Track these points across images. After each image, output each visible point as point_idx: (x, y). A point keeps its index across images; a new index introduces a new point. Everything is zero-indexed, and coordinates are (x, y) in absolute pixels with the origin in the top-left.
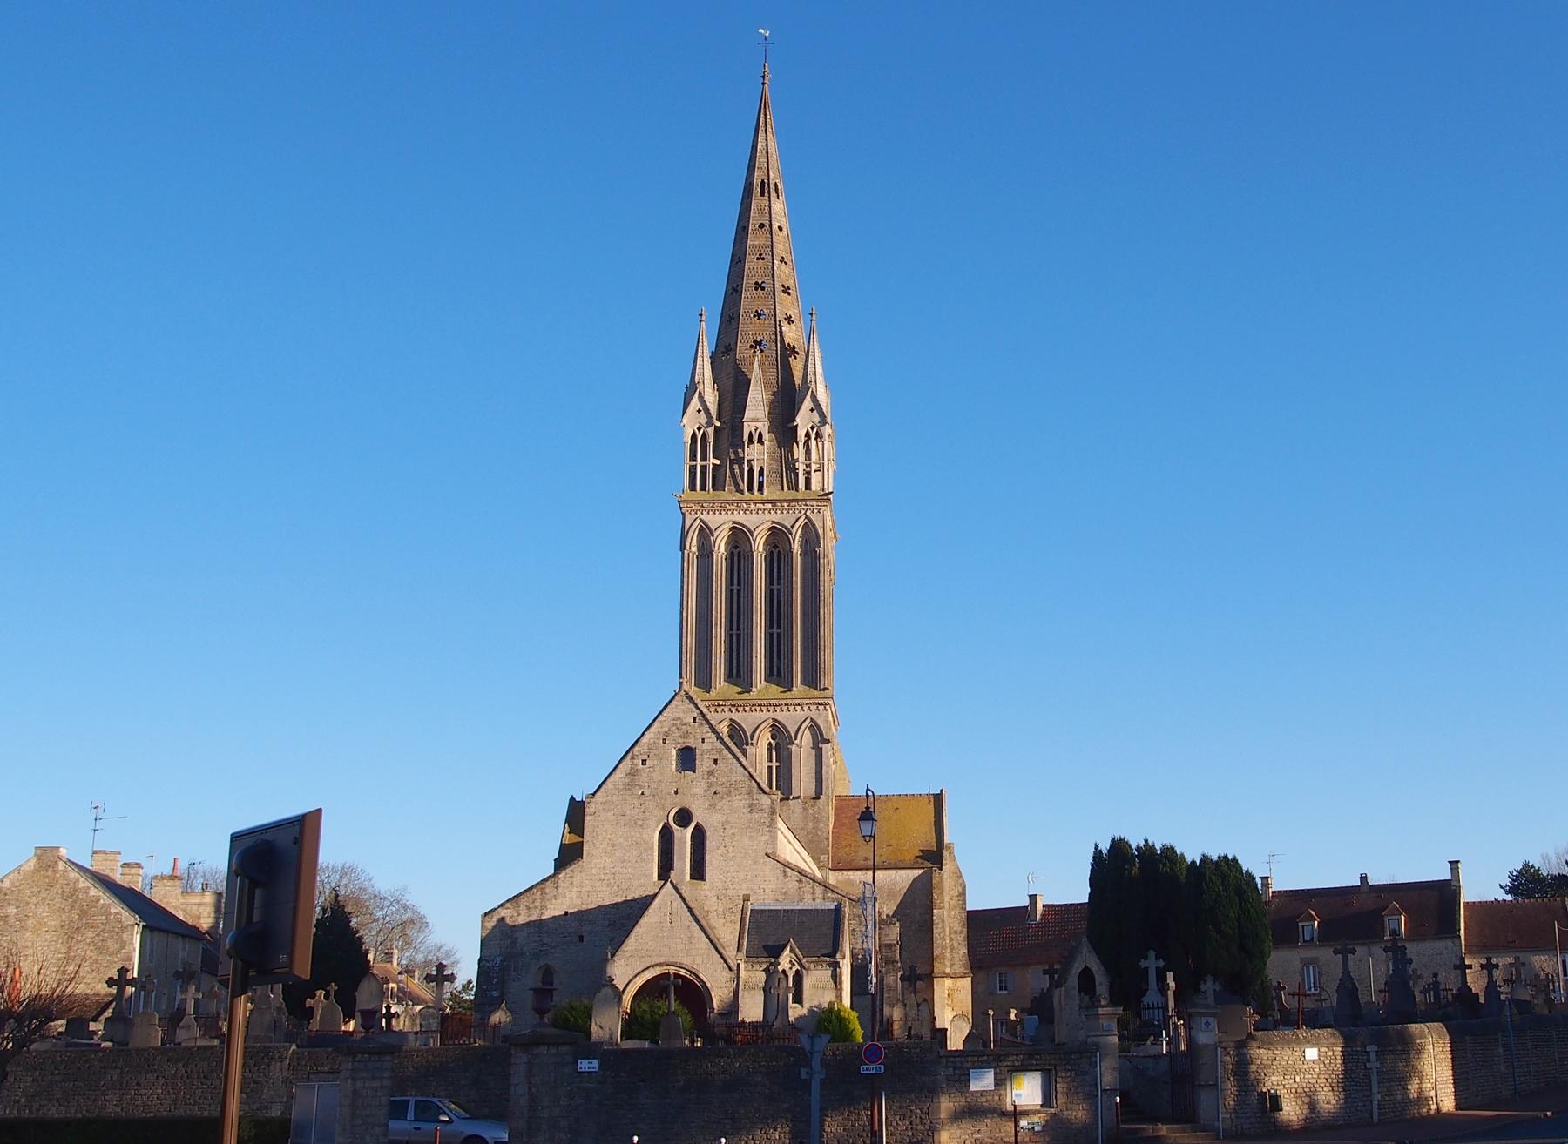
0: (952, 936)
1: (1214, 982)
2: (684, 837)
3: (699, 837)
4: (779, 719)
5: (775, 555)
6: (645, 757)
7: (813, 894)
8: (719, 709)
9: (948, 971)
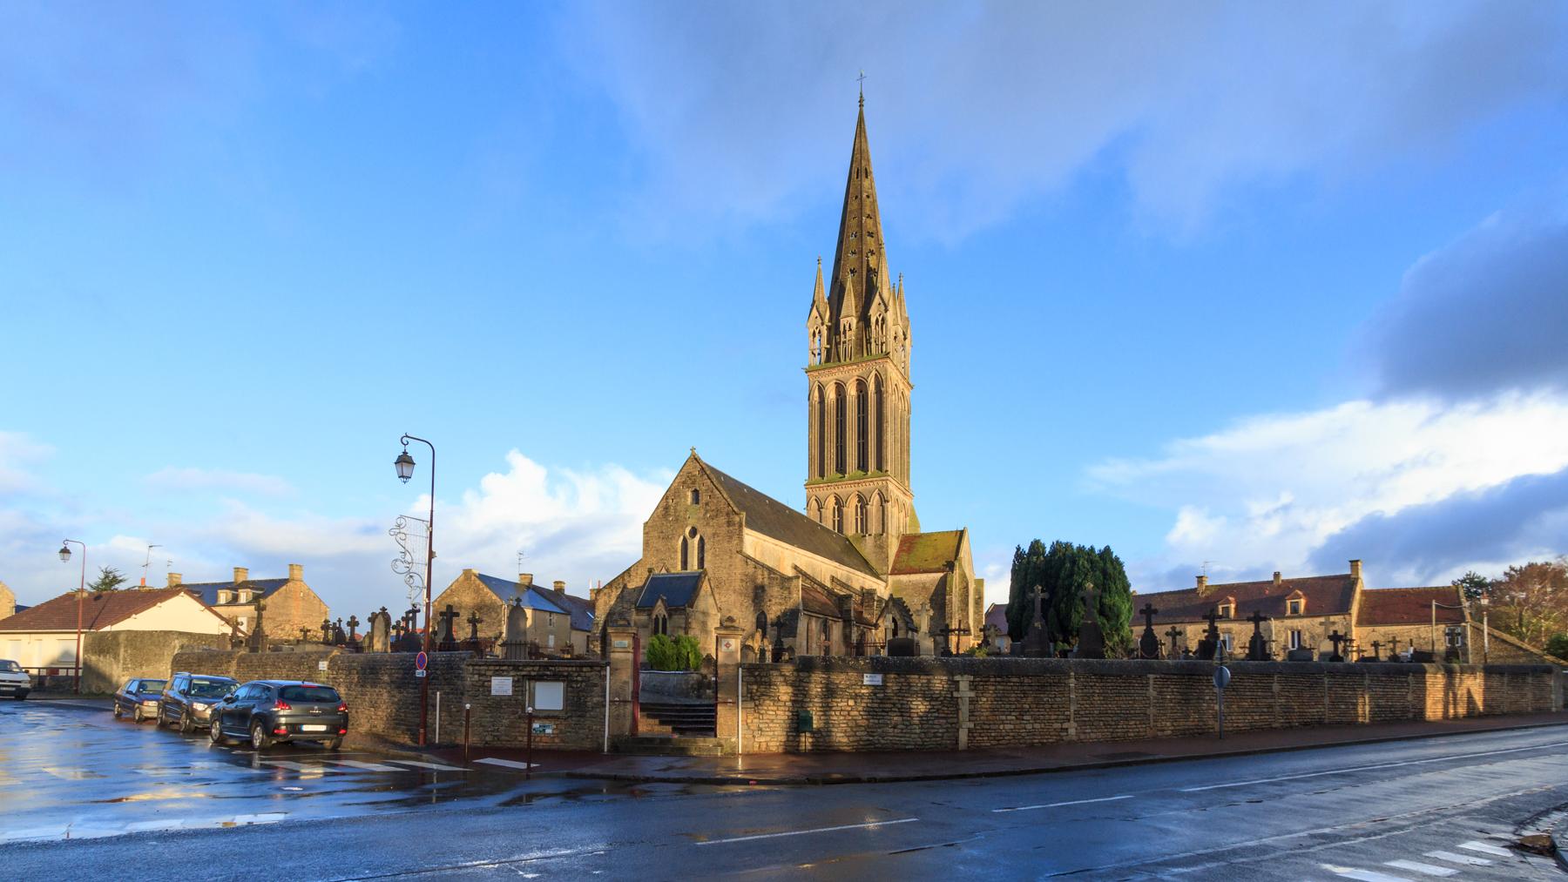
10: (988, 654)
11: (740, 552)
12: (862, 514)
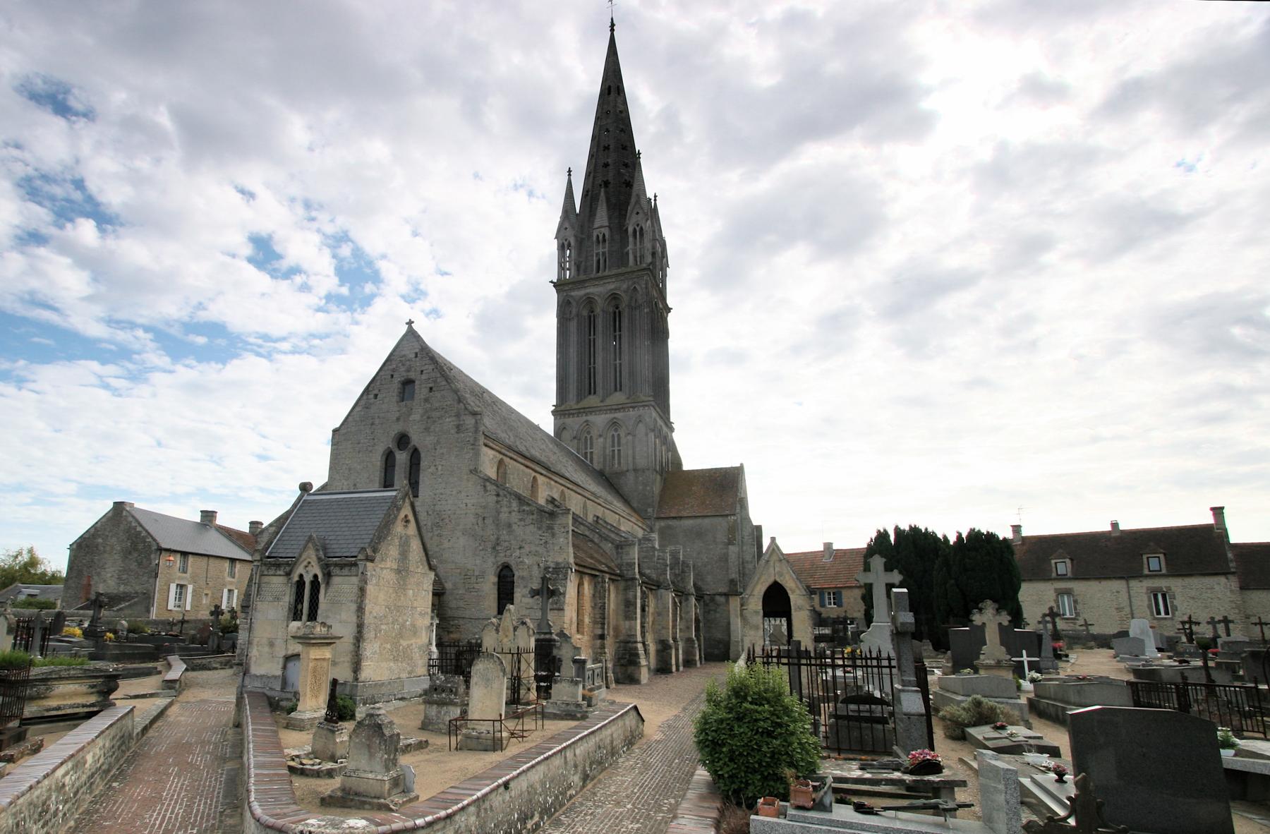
1: (998, 611)
2: (402, 458)
3: (415, 457)
6: (376, 392)
7: (510, 507)
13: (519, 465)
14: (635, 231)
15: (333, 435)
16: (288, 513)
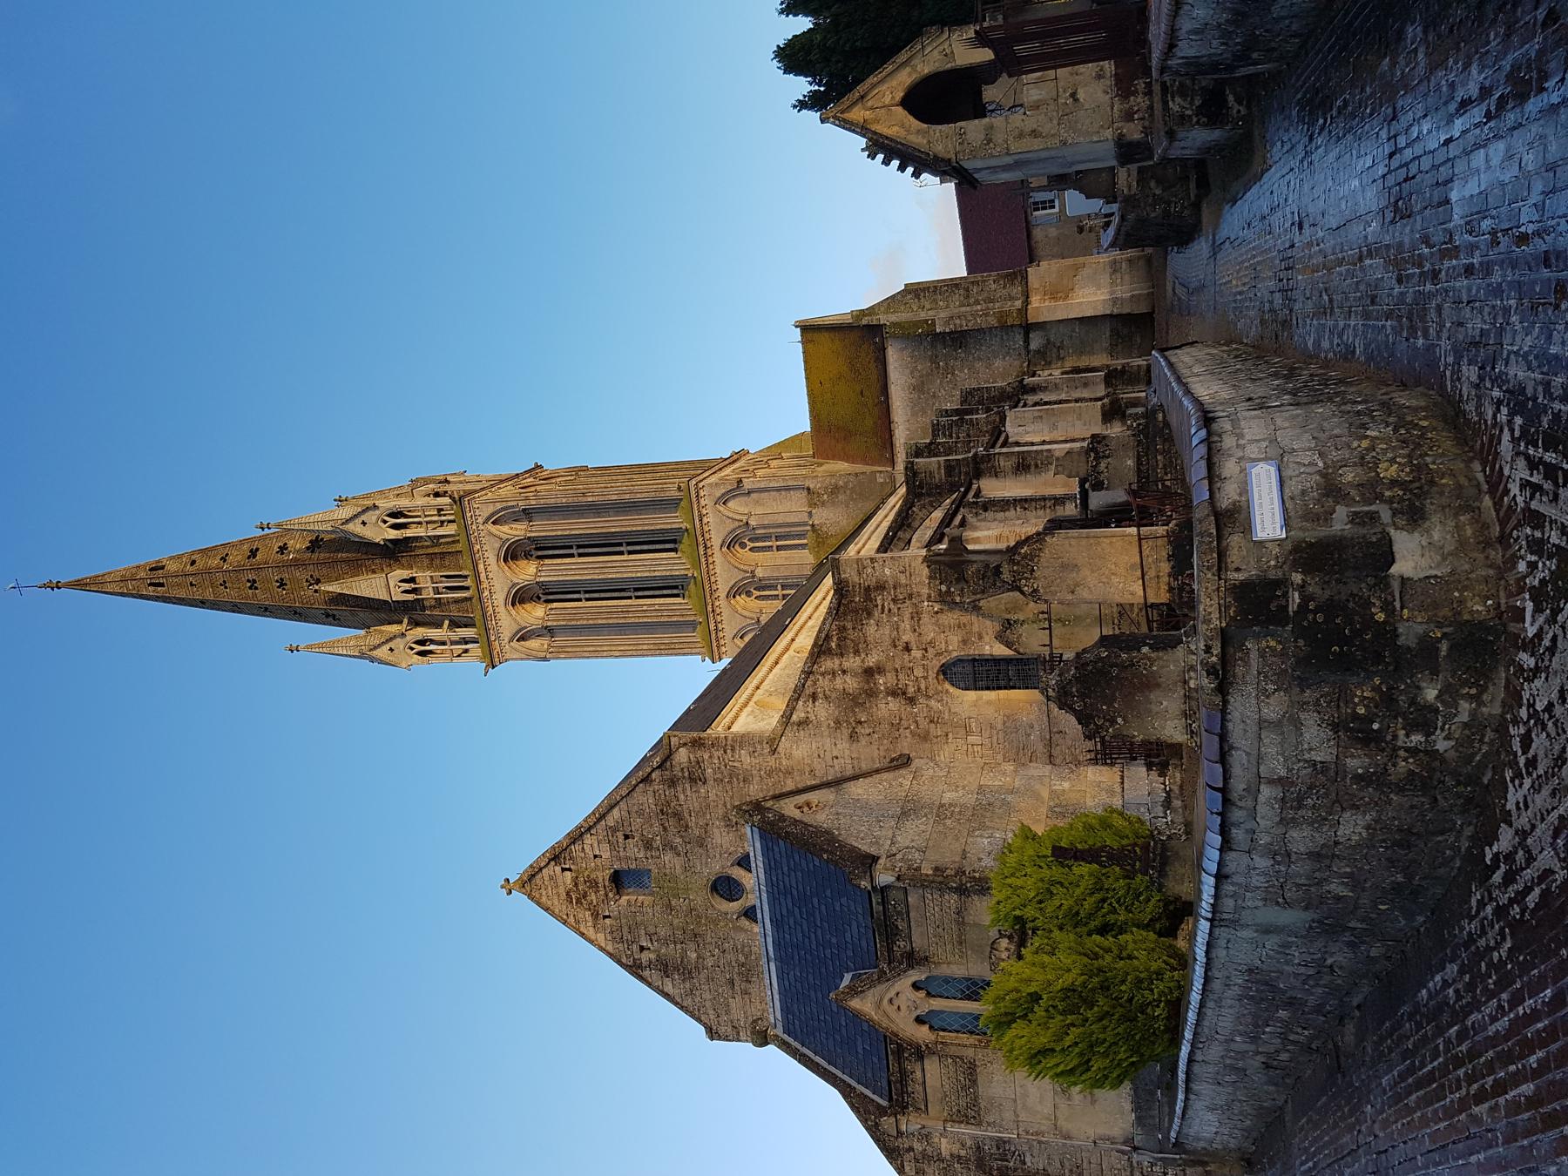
0: (972, 300)
4: (720, 541)
5: (540, 553)
6: (635, 948)
7: (834, 673)
8: (718, 610)
9: (1018, 304)
10: (1063, 373)
11: (773, 743)
12: (767, 537)
13: (771, 676)
14: (395, 527)
15: (719, 1038)
16: (847, 1093)
